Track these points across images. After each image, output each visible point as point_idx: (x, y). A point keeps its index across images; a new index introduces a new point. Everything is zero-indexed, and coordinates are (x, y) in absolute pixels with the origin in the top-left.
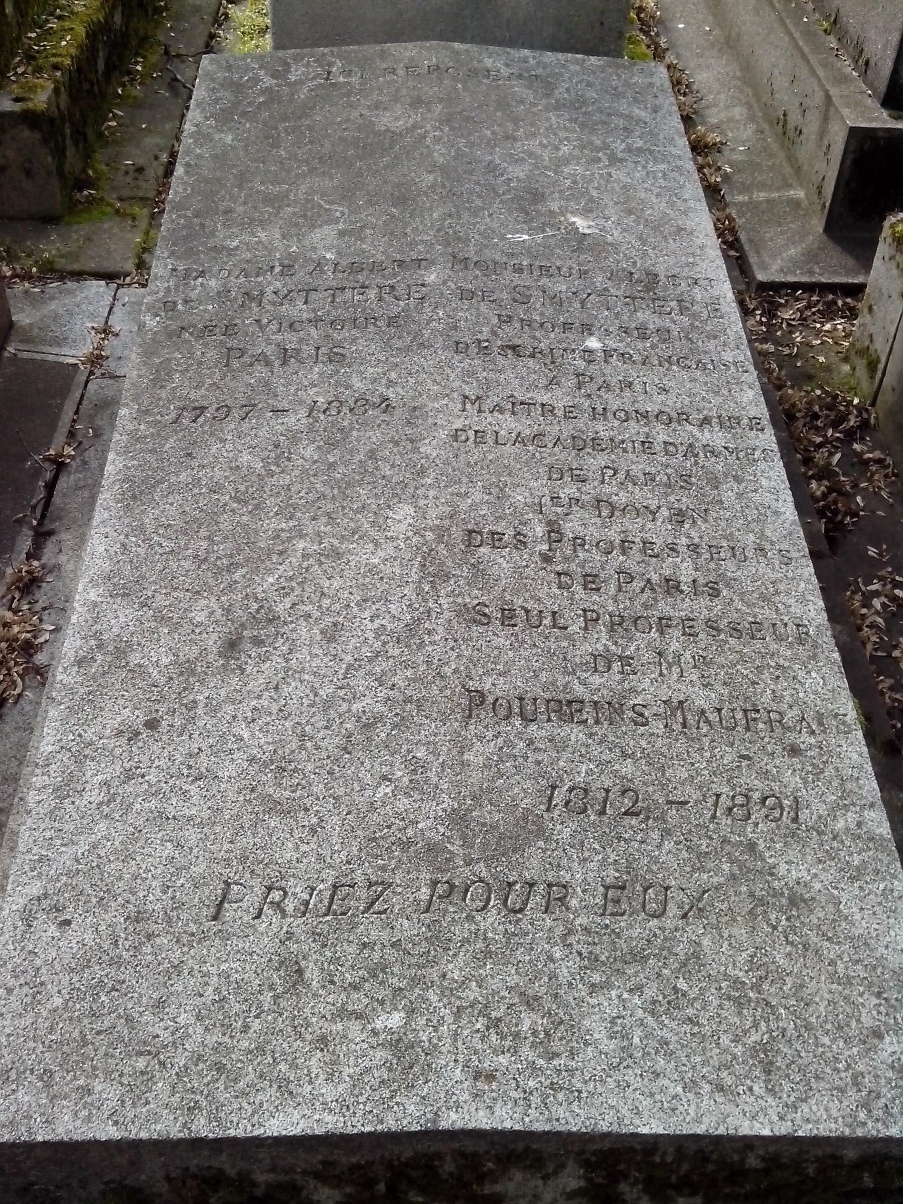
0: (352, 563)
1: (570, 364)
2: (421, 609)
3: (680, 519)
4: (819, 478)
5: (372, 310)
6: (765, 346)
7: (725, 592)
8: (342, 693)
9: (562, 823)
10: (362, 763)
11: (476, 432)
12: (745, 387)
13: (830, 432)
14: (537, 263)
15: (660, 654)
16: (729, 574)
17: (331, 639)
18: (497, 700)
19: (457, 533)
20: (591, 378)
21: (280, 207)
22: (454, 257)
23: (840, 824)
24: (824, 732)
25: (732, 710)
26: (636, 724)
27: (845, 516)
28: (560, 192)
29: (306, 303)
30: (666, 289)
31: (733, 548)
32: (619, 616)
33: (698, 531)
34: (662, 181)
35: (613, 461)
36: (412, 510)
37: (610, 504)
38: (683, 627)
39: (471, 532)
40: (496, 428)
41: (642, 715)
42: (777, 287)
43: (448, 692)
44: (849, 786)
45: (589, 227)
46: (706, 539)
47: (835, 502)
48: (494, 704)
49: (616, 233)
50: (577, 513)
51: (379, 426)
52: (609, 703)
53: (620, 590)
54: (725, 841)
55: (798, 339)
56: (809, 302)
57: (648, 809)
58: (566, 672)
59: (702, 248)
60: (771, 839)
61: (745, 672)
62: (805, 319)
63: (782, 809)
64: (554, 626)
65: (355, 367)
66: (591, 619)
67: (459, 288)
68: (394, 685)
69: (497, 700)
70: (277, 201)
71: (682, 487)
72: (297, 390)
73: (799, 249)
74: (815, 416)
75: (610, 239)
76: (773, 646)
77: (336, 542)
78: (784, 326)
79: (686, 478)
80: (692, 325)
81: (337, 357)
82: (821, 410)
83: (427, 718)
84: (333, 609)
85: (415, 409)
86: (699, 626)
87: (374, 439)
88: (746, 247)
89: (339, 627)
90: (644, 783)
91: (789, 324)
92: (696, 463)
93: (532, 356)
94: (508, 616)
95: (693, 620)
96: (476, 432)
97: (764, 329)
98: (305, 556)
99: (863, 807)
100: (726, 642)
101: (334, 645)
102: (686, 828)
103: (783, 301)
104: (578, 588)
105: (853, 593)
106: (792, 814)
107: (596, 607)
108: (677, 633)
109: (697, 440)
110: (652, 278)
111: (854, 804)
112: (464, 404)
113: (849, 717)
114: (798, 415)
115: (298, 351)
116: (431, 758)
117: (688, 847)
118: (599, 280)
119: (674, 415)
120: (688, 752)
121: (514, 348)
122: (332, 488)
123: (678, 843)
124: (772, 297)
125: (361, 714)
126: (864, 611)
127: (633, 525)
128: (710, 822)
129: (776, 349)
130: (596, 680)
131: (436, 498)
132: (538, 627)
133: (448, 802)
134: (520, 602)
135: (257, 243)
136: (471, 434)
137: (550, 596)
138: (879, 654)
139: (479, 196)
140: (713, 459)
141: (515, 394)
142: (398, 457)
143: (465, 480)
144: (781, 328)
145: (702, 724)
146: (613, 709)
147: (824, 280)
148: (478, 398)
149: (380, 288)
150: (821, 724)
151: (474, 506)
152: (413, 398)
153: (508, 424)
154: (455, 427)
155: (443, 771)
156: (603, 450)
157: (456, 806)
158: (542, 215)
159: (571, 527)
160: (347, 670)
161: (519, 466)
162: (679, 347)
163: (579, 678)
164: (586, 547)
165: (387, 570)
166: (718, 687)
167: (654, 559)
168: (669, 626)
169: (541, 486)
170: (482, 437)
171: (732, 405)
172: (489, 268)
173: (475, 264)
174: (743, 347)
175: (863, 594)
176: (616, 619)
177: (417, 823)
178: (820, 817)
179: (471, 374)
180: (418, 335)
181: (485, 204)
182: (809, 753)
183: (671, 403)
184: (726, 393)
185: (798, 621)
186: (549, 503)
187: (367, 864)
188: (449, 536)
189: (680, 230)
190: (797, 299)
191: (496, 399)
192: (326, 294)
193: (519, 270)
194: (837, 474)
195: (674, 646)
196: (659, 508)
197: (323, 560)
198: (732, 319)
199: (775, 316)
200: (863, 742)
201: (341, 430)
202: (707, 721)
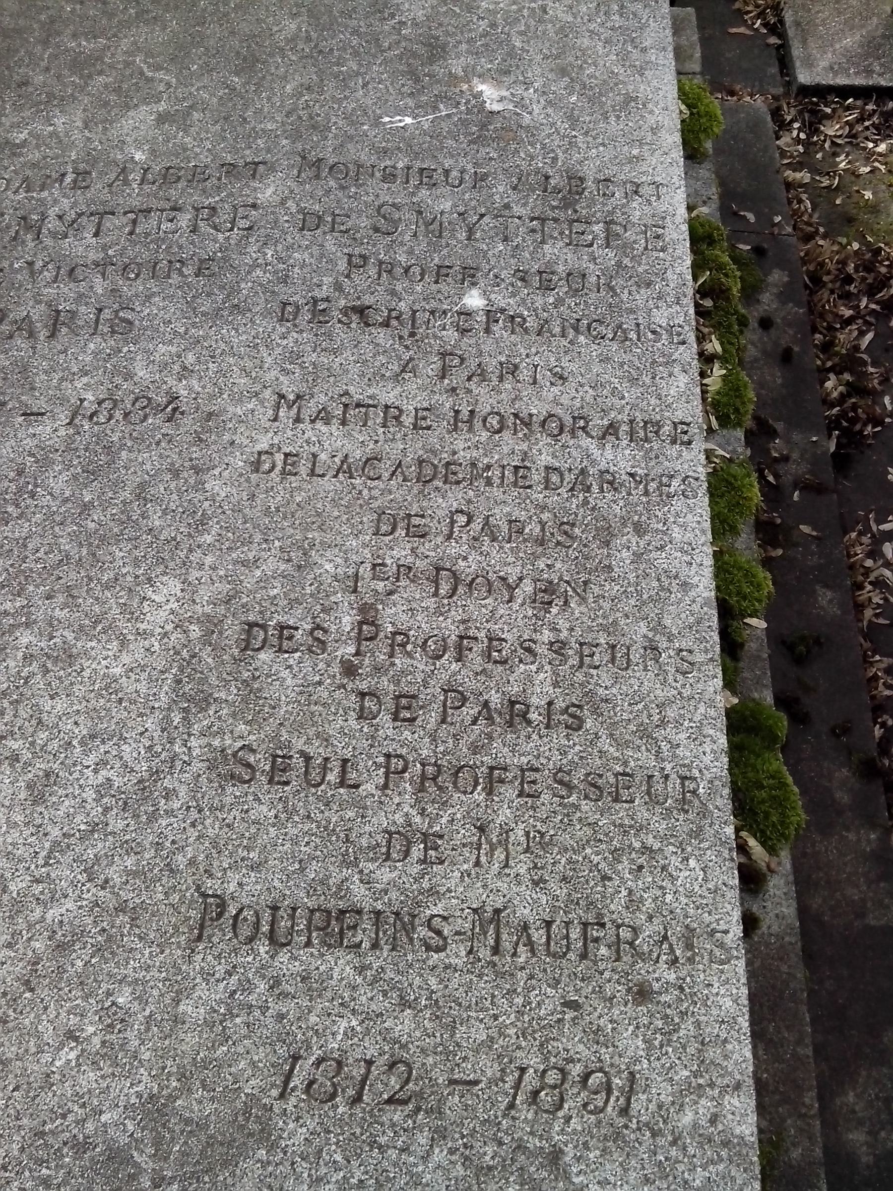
0: (86, 674)
1: (435, 337)
2: (164, 754)
3: (547, 598)
4: (837, 370)
5: (180, 247)
6: (798, 175)
7: (589, 723)
8: (37, 889)
9: (297, 1120)
10: (46, 1008)
11: (286, 455)
12: (677, 370)
13: (864, 303)
14: (418, 164)
15: (482, 829)
16: (601, 691)
17: (38, 799)
18: (241, 910)
19: (232, 630)
20: (462, 360)
21: (90, 76)
22: (304, 158)
23: (688, 1118)
24: (691, 960)
25: (567, 924)
26: (428, 948)
27: (865, 425)
28: (470, 41)
29: (96, 235)
30: (592, 202)
31: (613, 647)
32: (435, 764)
33: (570, 620)
34: (616, 17)
35: (469, 502)
36: (179, 586)
37: (454, 573)
38: (522, 784)
39: (252, 625)
40: (315, 449)
41: (439, 933)
42: (821, 92)
43: (175, 898)
44: (712, 1053)
45: (501, 100)
46: (578, 631)
47: (854, 408)
48: (236, 917)
49: (537, 109)
50: (408, 590)
51: (158, 443)
52: (397, 914)
53: (443, 721)
54: (520, 1147)
55: (842, 165)
56: (862, 114)
57: (420, 1095)
58: (346, 863)
59: (654, 130)
60: (585, 1144)
61: (596, 859)
62: (854, 136)
63: (609, 1092)
64: (342, 784)
65: (143, 344)
66: (393, 770)
67: (301, 211)
68: (106, 881)
69: (241, 910)
70: (84, 65)
71: (558, 543)
72: (62, 379)
73: (858, 37)
74: (849, 280)
75: (527, 119)
76: (643, 814)
77: (70, 636)
78: (827, 145)
79: (566, 527)
80: (619, 264)
81: (122, 328)
82: (856, 270)
83: (141, 939)
84: (49, 748)
85: (210, 414)
86: (544, 779)
87: (148, 467)
88: (791, 32)
89: (52, 780)
90: (423, 1051)
91: (833, 142)
92: (586, 502)
93: (386, 324)
94: (278, 771)
95: (537, 770)
96: (286, 455)
97: (801, 148)
98: (28, 658)
99: (724, 1090)
100: (577, 807)
101: (39, 809)
102: (469, 1124)
103: (829, 110)
104: (384, 718)
105: (861, 534)
106: (622, 1100)
107: (404, 751)
108: (510, 792)
109: (593, 462)
110: (576, 181)
111: (712, 1085)
112: (278, 407)
113: (731, 935)
114: (825, 278)
115: (73, 314)
116: (136, 1007)
117: (467, 1158)
118: (500, 190)
119: (568, 420)
120: (493, 996)
121: (361, 311)
122: (81, 545)
123: (452, 1151)
124: (817, 104)
125: (56, 927)
126: (869, 563)
127: (478, 608)
128: (504, 1116)
129: (813, 179)
130: (385, 875)
131: (214, 568)
132: (319, 785)
133: (146, 1083)
134: (299, 744)
135: (51, 134)
136: (279, 458)
137: (343, 734)
138: (881, 621)
139: (356, 54)
140: (609, 496)
141: (352, 389)
142: (175, 497)
143: (258, 537)
144: (822, 148)
145: (521, 949)
146: (399, 926)
147: (883, 83)
148: (299, 397)
149: (197, 210)
150: (689, 946)
151: (264, 582)
152: (211, 397)
153: (335, 441)
154: (259, 447)
155: (148, 1030)
156: (458, 483)
157: (155, 1091)
158: (438, 82)
159: (392, 616)
160: (51, 851)
161: (336, 513)
162: (594, 302)
163: (361, 872)
164: (409, 647)
165: (128, 686)
166: (552, 885)
167: (500, 668)
168: (502, 781)
169: (360, 547)
170: (293, 464)
171: (653, 401)
172: (351, 174)
173: (331, 168)
174: (685, 301)
175: (873, 536)
176: (430, 769)
177: (101, 1112)
178: (660, 1107)
179: (295, 357)
180: (234, 290)
181: (361, 65)
182: (664, 998)
183: (564, 399)
184: (648, 381)
185: (684, 772)
186: (368, 575)
187: (27, 1173)
188: (221, 633)
189: (629, 99)
190: (848, 108)
191: (323, 398)
192: (124, 220)
193: (389, 176)
194: (865, 364)
195: (505, 814)
196: (521, 579)
197: (49, 665)
198: (678, 252)
199: (817, 131)
200: (744, 980)
201: (108, 449)
202: (530, 944)
